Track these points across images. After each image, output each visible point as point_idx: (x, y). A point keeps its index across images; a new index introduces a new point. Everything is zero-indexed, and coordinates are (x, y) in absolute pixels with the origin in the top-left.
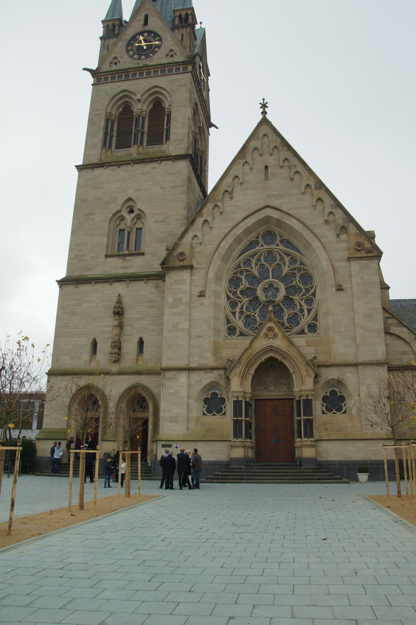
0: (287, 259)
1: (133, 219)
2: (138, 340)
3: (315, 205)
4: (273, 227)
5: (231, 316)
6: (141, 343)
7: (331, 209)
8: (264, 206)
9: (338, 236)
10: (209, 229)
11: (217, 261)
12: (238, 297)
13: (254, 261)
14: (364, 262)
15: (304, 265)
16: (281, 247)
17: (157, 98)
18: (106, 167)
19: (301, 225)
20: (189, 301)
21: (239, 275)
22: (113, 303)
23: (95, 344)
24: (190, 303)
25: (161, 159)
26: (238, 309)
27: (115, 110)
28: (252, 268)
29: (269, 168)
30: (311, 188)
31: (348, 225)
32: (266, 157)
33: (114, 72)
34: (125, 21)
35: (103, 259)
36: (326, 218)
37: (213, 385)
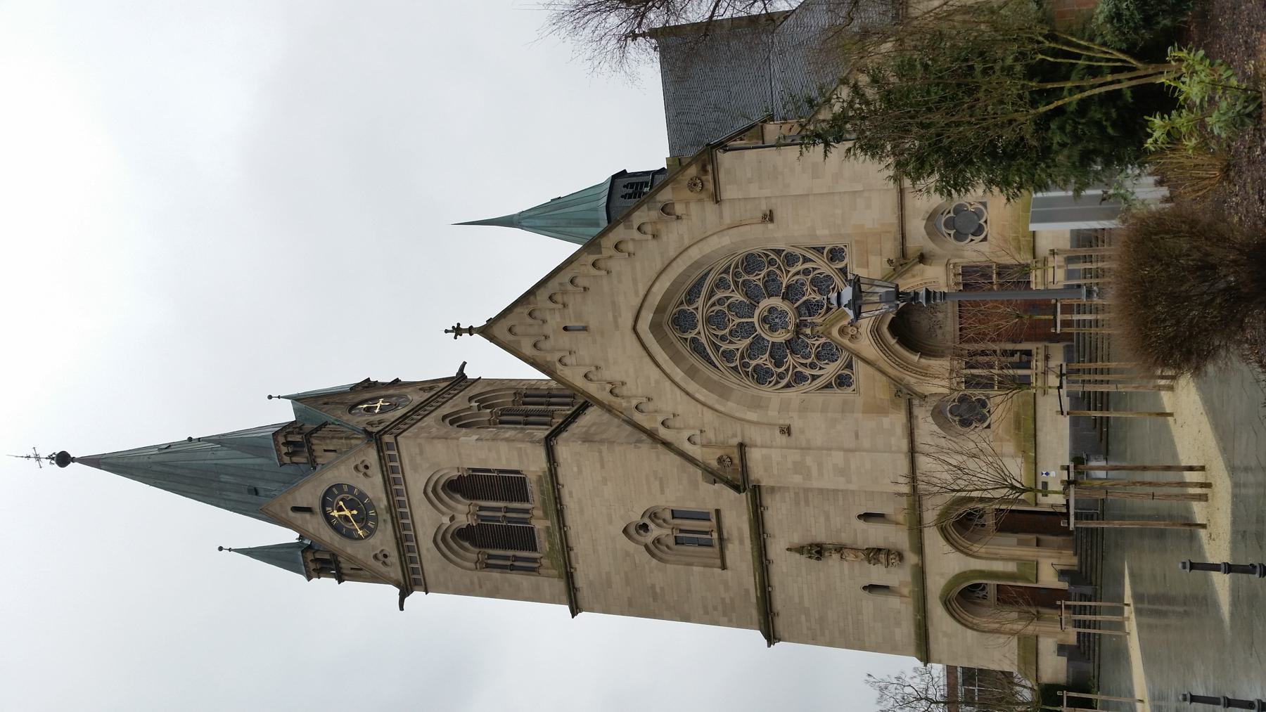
0: (720, 295)
1: (658, 525)
2: (862, 521)
3: (627, 254)
4: (667, 317)
5: (819, 382)
6: (866, 517)
7: (633, 229)
8: (634, 335)
9: (678, 218)
10: (678, 418)
11: (730, 407)
12: (787, 370)
13: (725, 346)
14: (722, 177)
15: (729, 267)
16: (700, 302)
17: (443, 488)
18: (572, 568)
19: (664, 276)
20: (799, 451)
21: (750, 369)
22: (803, 559)
23: (871, 588)
24: (802, 449)
25: (555, 485)
26: (807, 372)
27: (468, 555)
28: (738, 349)
29: (567, 325)
30: (598, 260)
31: (660, 202)
32: (548, 329)
33: (403, 559)
34: (299, 539)
35: (728, 574)
36: (650, 237)
37: (937, 414)
